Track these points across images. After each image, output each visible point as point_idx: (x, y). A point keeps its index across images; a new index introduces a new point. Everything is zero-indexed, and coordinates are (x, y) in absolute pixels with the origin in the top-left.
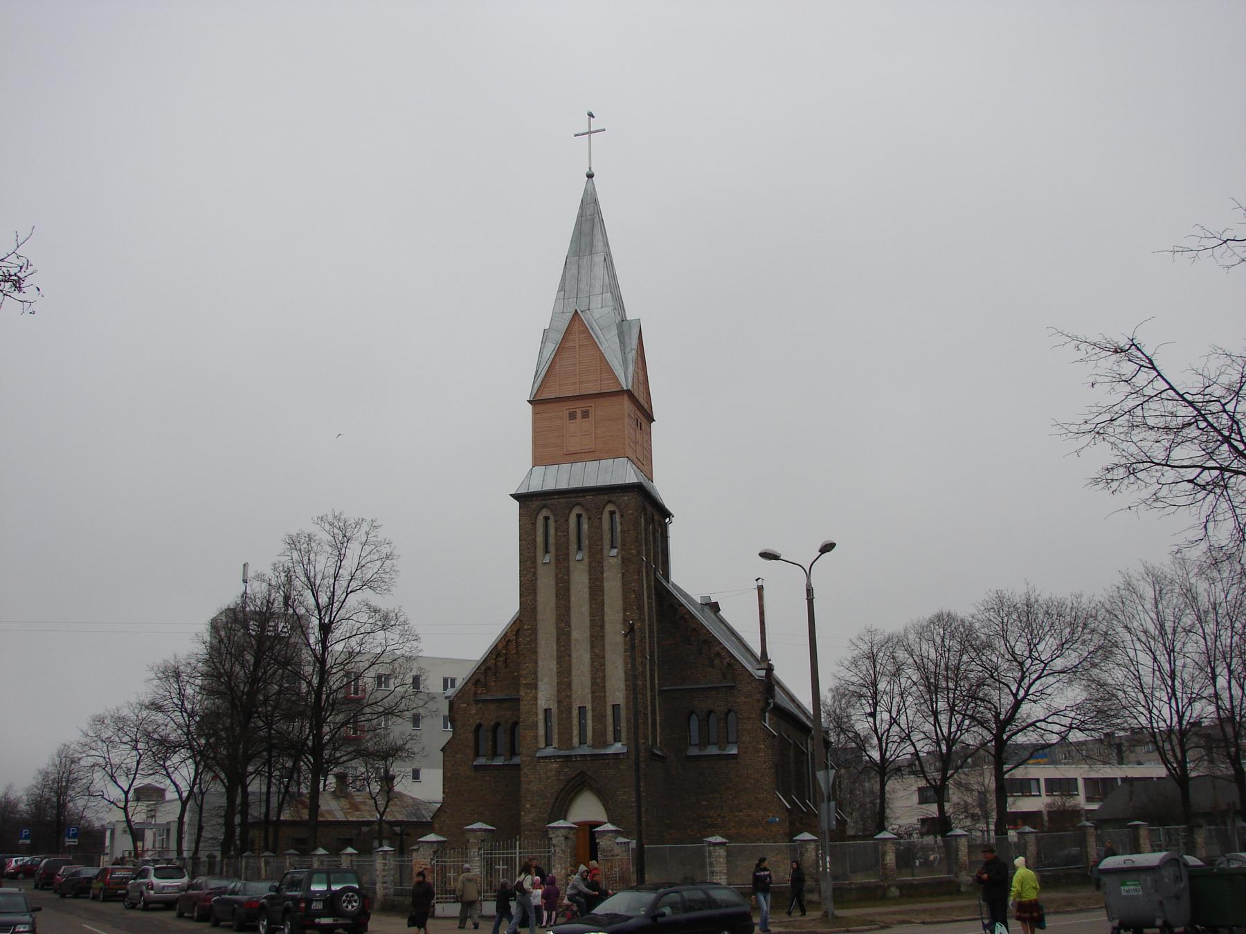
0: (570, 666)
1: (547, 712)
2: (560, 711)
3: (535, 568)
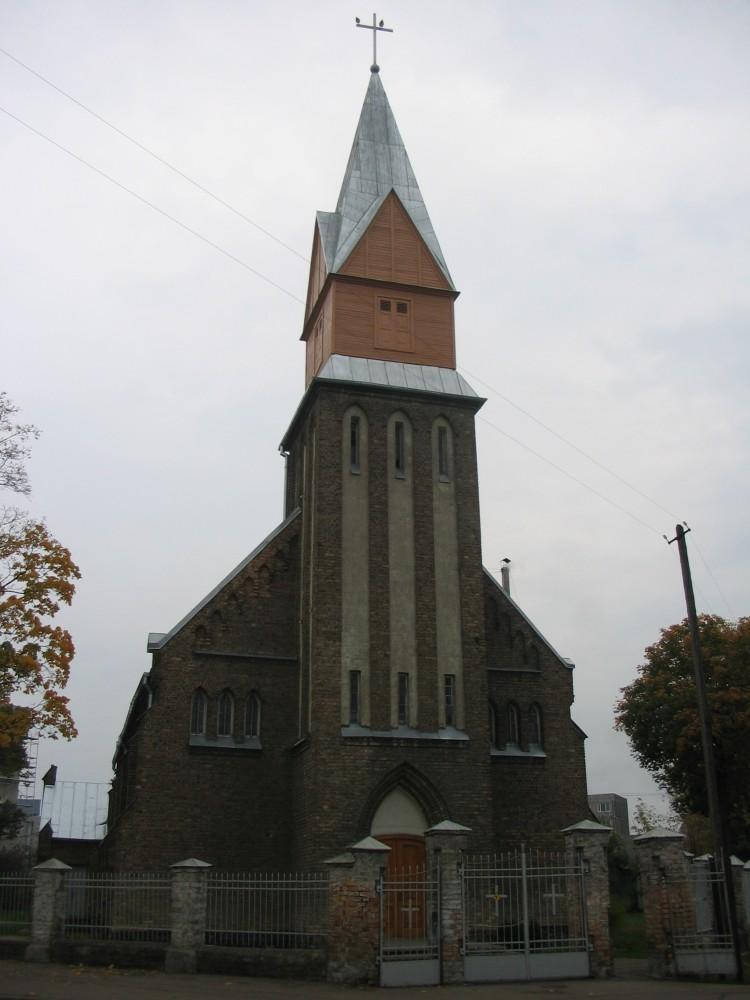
0: (388, 615)
1: (355, 675)
2: (373, 675)
3: (340, 478)
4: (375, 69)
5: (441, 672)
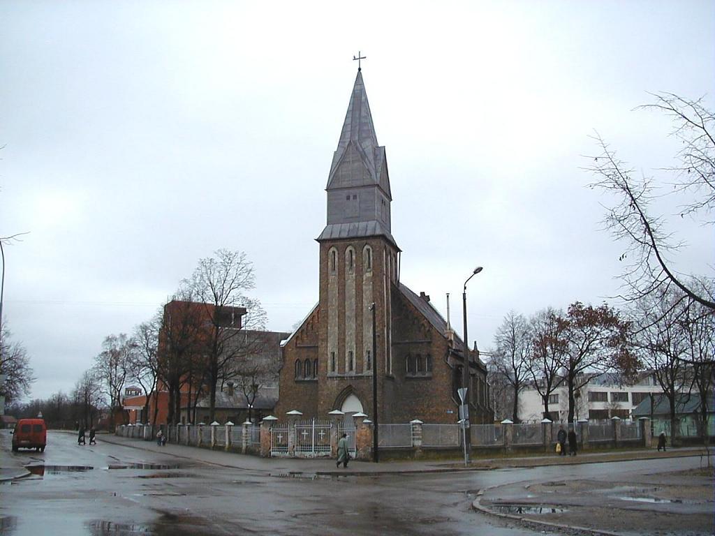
4: (360, 69)
5: (365, 349)
